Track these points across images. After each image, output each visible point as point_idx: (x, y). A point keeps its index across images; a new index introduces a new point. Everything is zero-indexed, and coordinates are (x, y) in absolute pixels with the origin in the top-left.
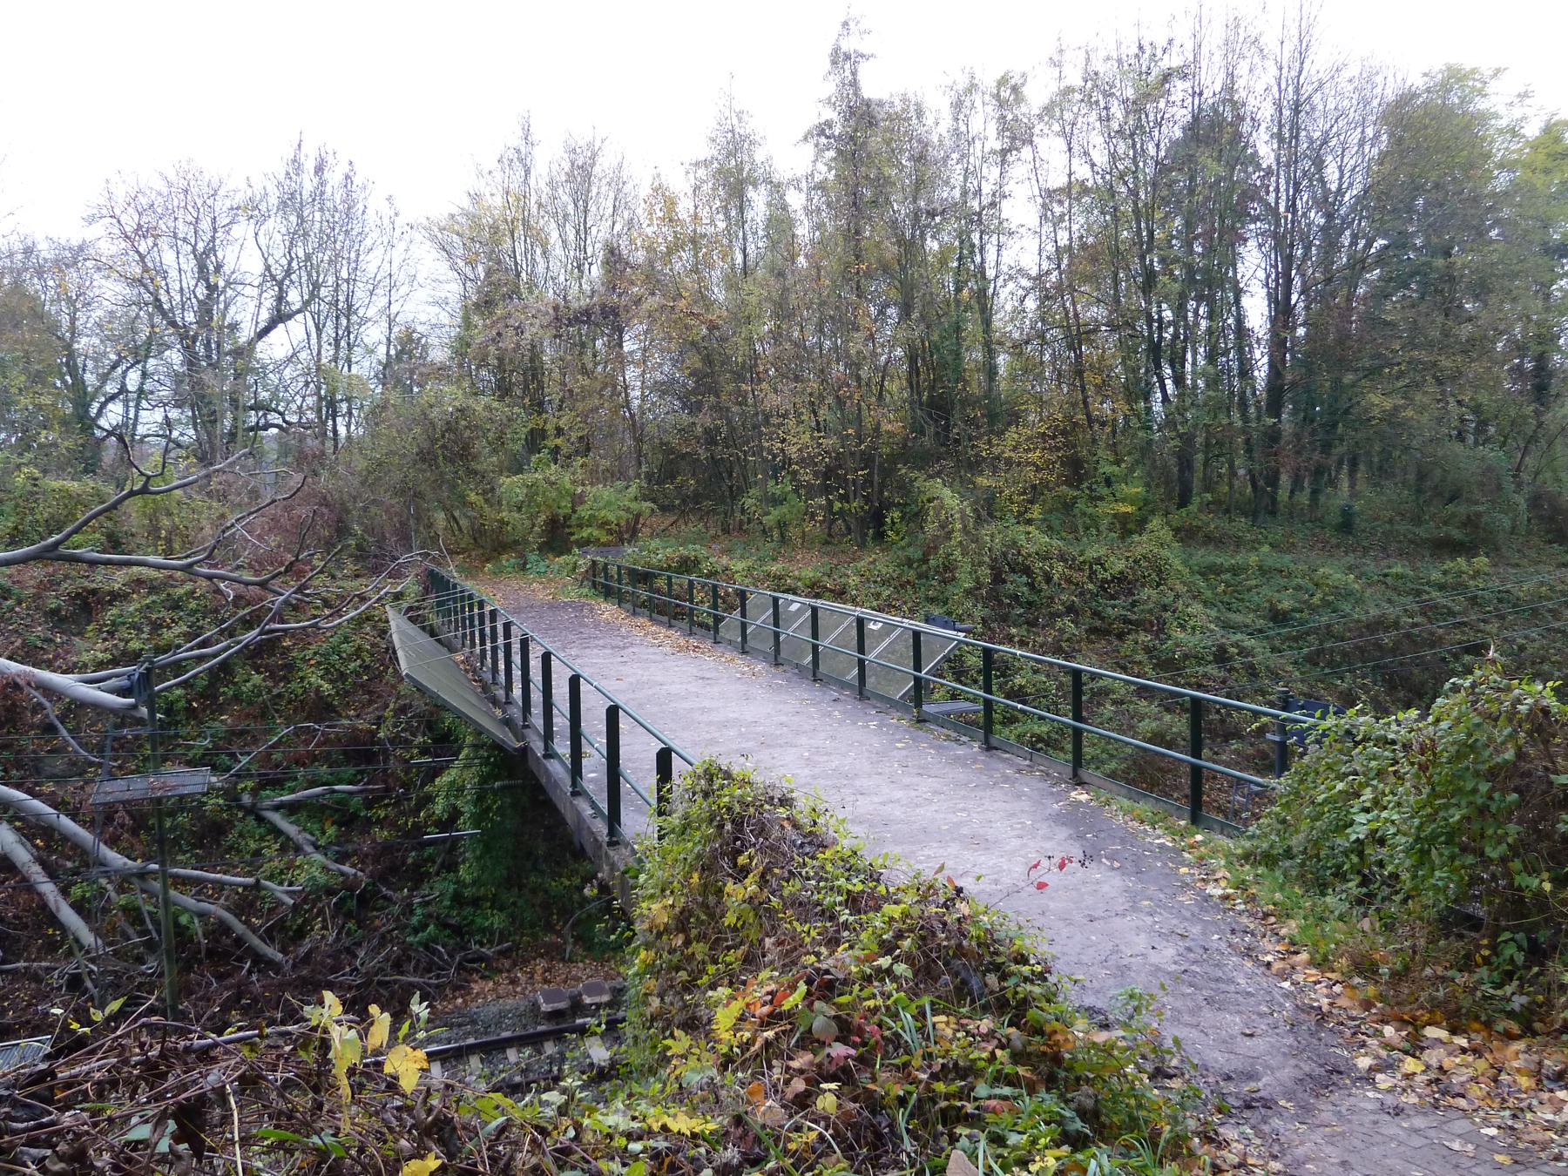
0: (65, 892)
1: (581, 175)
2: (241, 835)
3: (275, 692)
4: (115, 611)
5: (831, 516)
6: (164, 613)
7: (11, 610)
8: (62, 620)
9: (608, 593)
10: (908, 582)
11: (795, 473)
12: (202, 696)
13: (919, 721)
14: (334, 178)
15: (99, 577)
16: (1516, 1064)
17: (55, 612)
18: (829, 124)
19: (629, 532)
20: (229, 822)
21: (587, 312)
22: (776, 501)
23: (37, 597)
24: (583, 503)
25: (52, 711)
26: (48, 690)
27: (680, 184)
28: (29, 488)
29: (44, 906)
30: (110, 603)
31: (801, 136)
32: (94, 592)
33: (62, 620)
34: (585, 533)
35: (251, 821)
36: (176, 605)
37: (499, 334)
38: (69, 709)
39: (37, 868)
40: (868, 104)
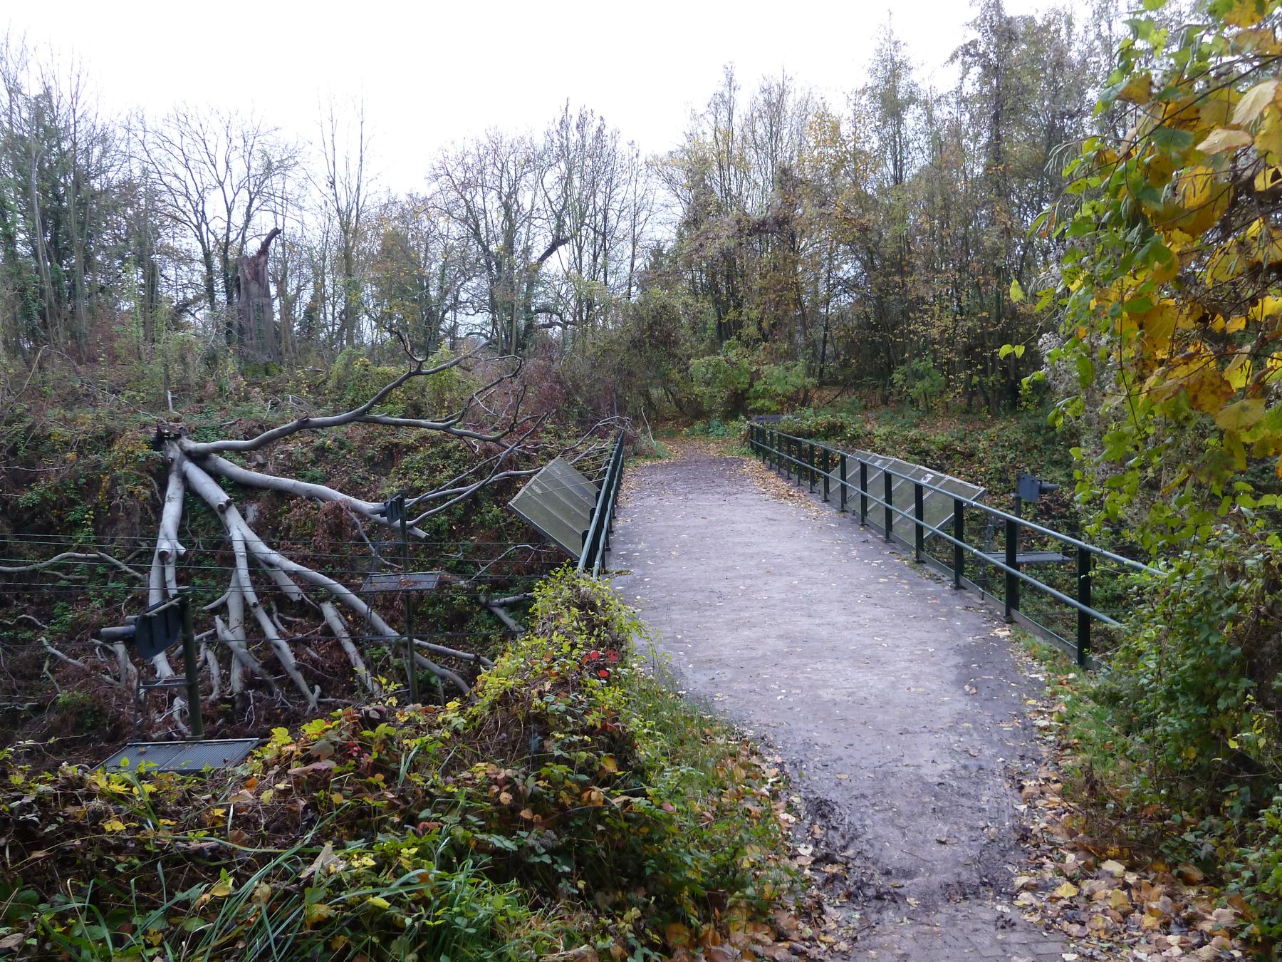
0: (361, 653)
1: (774, 109)
2: (477, 623)
3: (509, 520)
4: (408, 459)
5: (970, 392)
6: (439, 461)
7: (344, 457)
8: (376, 464)
9: (759, 451)
10: (1036, 447)
11: (935, 351)
12: (460, 521)
13: (918, 562)
14: (591, 131)
15: (402, 433)
16: (1153, 905)
17: (371, 458)
18: (974, 44)
19: (799, 399)
20: (470, 613)
21: (764, 223)
22: (919, 376)
23: (361, 448)
24: (759, 379)
25: (362, 529)
26: (356, 510)
27: (841, 109)
28: (362, 372)
29: (348, 662)
30: (406, 453)
31: (947, 58)
32: (396, 445)
33: (376, 464)
34: (759, 403)
35: (484, 614)
36: (447, 455)
37: (701, 245)
38: (373, 527)
39: (345, 635)
40: (1010, 21)
